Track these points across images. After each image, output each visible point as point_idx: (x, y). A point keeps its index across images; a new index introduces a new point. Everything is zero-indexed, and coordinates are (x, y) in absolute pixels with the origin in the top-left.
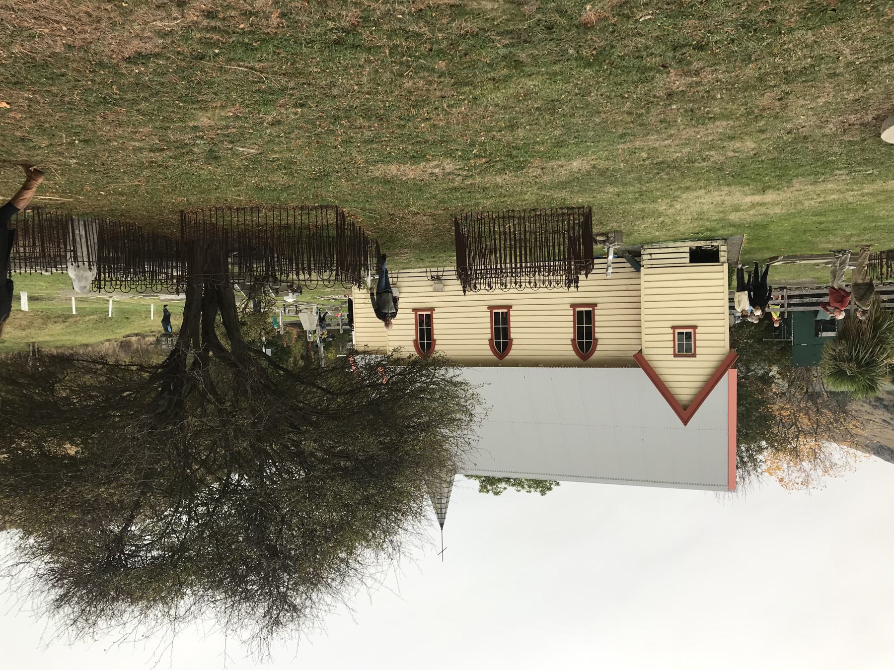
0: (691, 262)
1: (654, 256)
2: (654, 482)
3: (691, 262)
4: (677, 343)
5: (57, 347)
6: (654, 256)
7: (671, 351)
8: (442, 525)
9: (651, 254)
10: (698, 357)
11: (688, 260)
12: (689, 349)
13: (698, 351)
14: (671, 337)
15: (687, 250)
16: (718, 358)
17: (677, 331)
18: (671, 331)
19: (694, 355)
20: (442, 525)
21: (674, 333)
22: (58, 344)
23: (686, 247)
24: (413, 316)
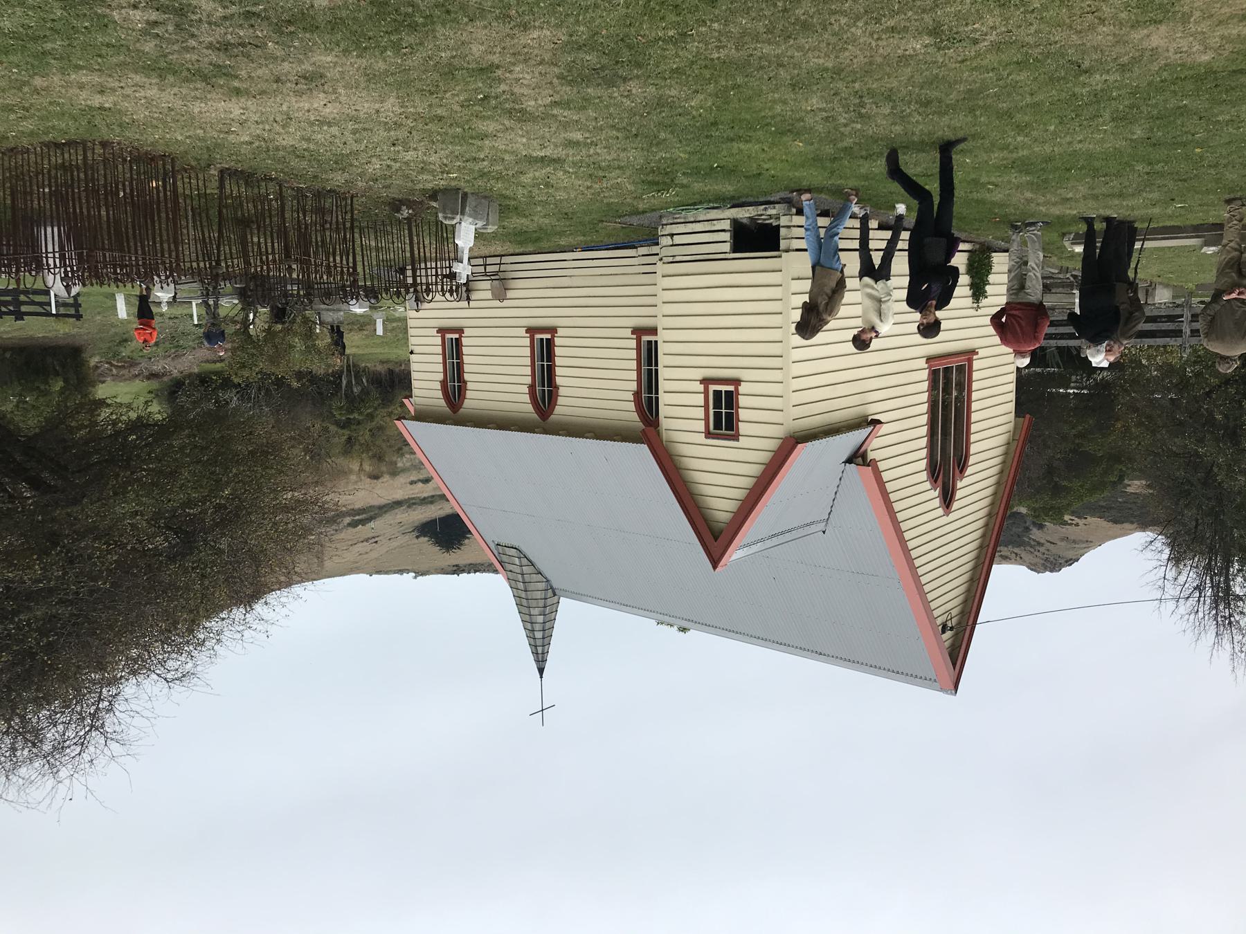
0: (735, 249)
1: (677, 240)
2: (819, 654)
3: (735, 249)
4: (711, 411)
5: (382, 362)
6: (677, 240)
7: (701, 426)
8: (541, 671)
9: (672, 235)
10: (743, 442)
11: (727, 247)
12: (730, 426)
13: (743, 428)
14: (700, 399)
15: (726, 225)
16: (1002, 440)
17: (713, 388)
18: (701, 388)
19: (736, 437)
20: (541, 671)
21: (706, 392)
22: (381, 357)
23: (724, 217)
24: (439, 340)
